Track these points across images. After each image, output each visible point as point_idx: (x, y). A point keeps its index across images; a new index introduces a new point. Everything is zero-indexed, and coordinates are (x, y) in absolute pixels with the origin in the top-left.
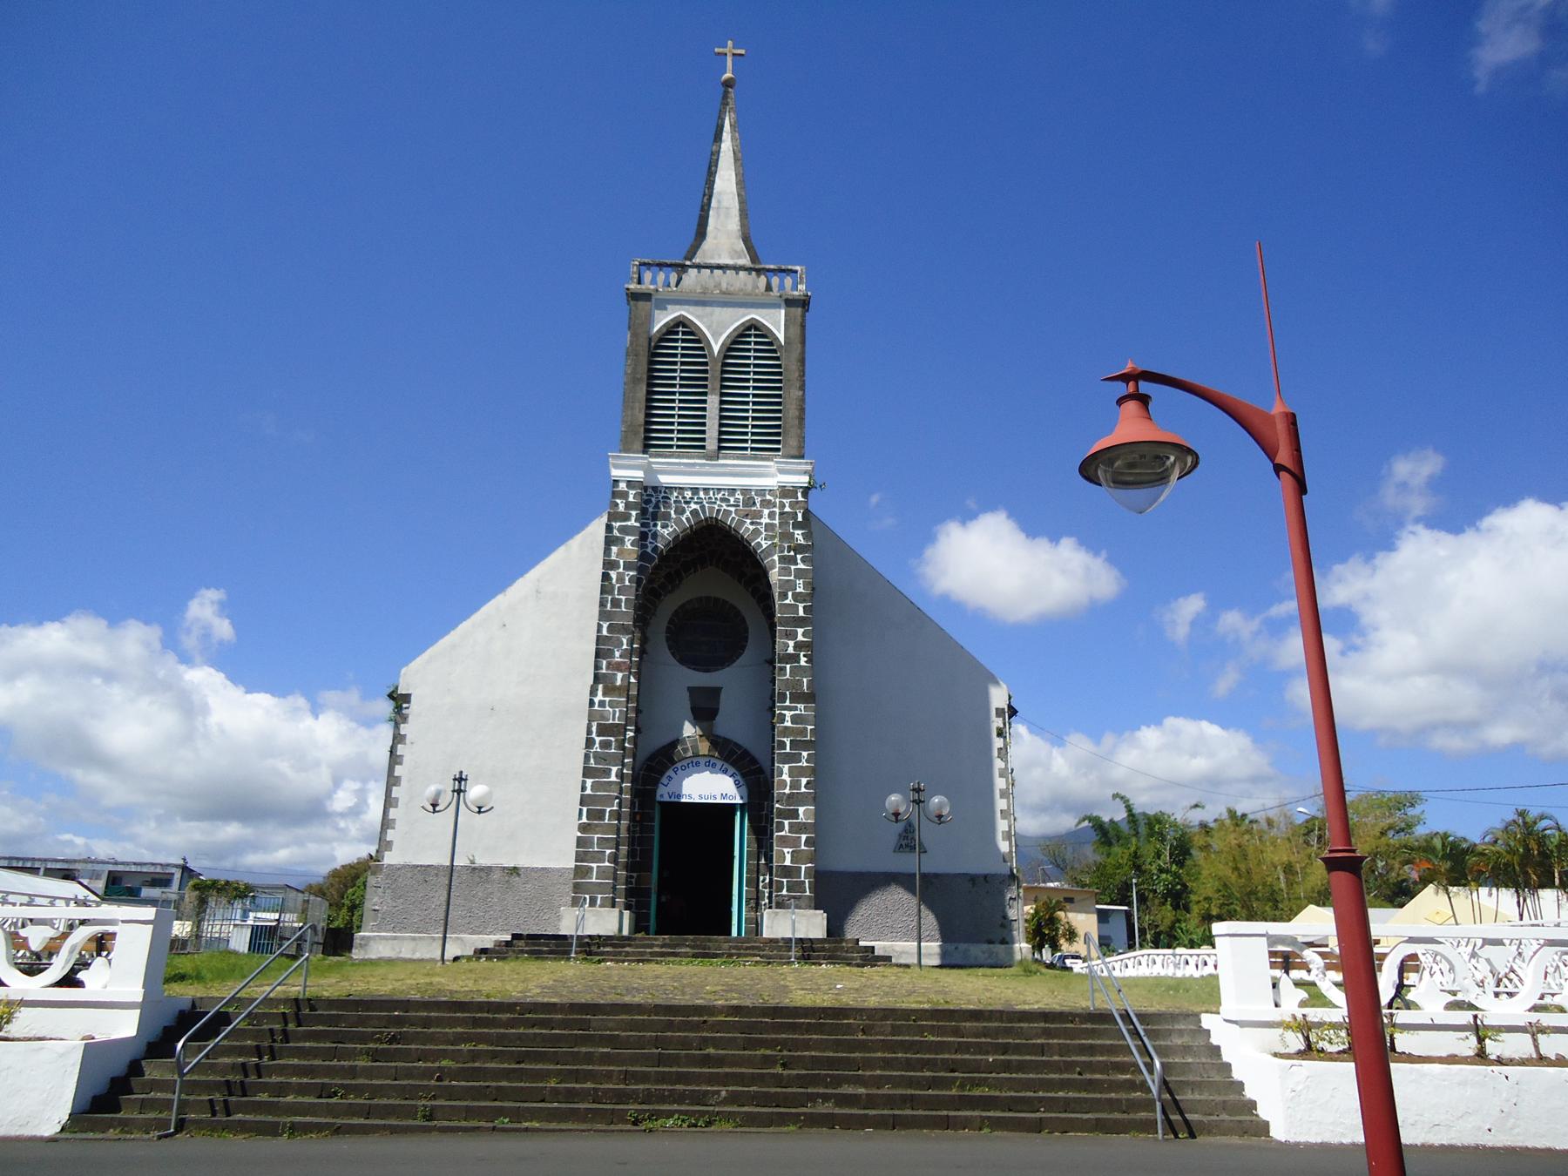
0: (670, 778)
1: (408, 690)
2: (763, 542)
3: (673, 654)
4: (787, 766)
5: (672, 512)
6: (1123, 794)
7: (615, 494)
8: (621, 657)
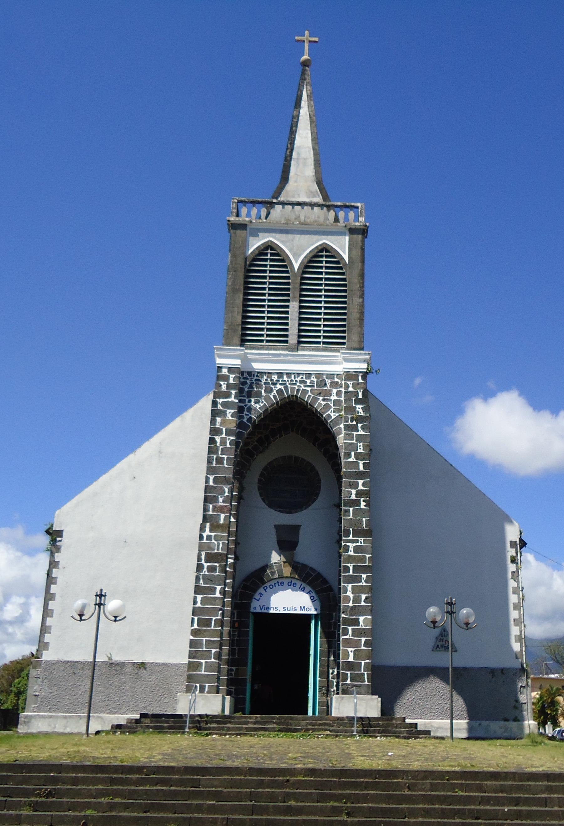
0: (261, 595)
1: (61, 527)
2: (332, 414)
3: (263, 500)
4: (350, 586)
5: (263, 391)
7: (219, 378)
8: (223, 502)
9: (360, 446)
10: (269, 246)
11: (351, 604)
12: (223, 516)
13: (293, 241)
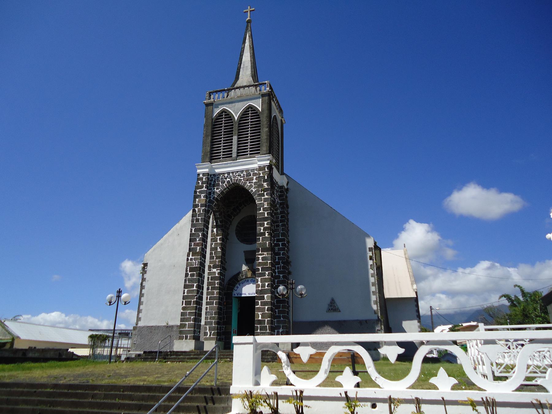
0: (238, 287)
1: (147, 261)
2: (253, 190)
3: (238, 239)
4: (260, 278)
5: (220, 183)
6: (519, 285)
7: (198, 179)
8: (199, 241)
9: (265, 204)
10: (224, 111)
11: (260, 289)
12: (198, 248)
13: (235, 107)
